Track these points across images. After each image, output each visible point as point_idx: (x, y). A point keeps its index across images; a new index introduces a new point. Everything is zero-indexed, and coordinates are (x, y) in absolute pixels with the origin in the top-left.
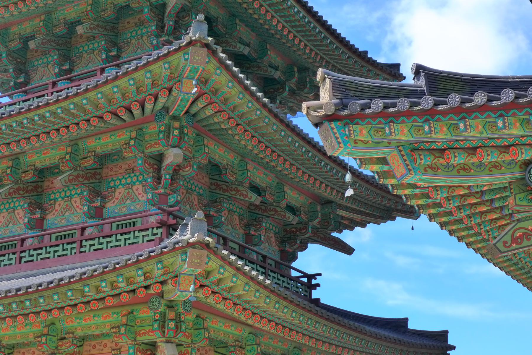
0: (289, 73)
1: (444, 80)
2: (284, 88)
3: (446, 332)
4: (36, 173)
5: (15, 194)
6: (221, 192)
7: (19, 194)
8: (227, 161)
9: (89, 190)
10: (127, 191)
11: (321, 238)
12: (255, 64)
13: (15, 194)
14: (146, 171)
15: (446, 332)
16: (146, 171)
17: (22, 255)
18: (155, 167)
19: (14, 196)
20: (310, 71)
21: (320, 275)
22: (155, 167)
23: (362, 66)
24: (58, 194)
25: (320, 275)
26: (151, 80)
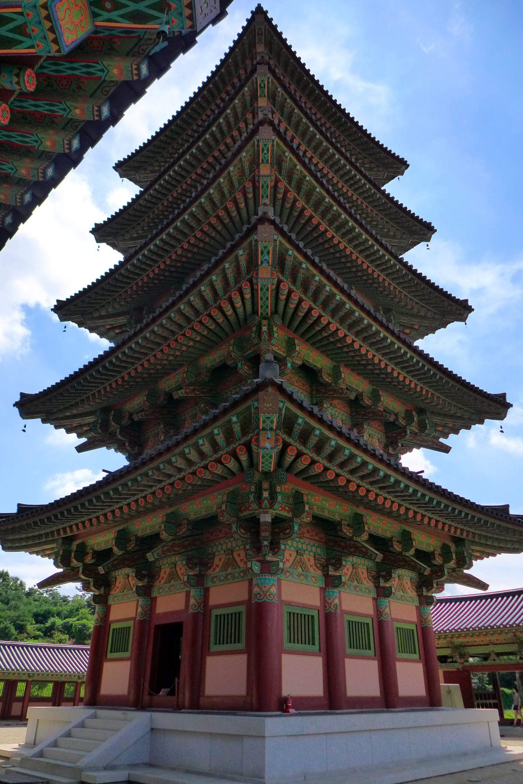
0: (409, 416)
1: (229, 634)
2: (406, 432)
3: (508, 506)
4: (138, 543)
5: (170, 552)
6: (339, 549)
7: (175, 551)
8: (340, 516)
9: (187, 560)
10: (227, 557)
11: (454, 577)
12: (331, 388)
13: (170, 552)
14: (242, 537)
15: (508, 506)
16: (242, 537)
18: (253, 530)
19: (168, 554)
20: (428, 412)
22: (253, 530)
23: (483, 402)
24: (220, 546)
26: (317, 438)
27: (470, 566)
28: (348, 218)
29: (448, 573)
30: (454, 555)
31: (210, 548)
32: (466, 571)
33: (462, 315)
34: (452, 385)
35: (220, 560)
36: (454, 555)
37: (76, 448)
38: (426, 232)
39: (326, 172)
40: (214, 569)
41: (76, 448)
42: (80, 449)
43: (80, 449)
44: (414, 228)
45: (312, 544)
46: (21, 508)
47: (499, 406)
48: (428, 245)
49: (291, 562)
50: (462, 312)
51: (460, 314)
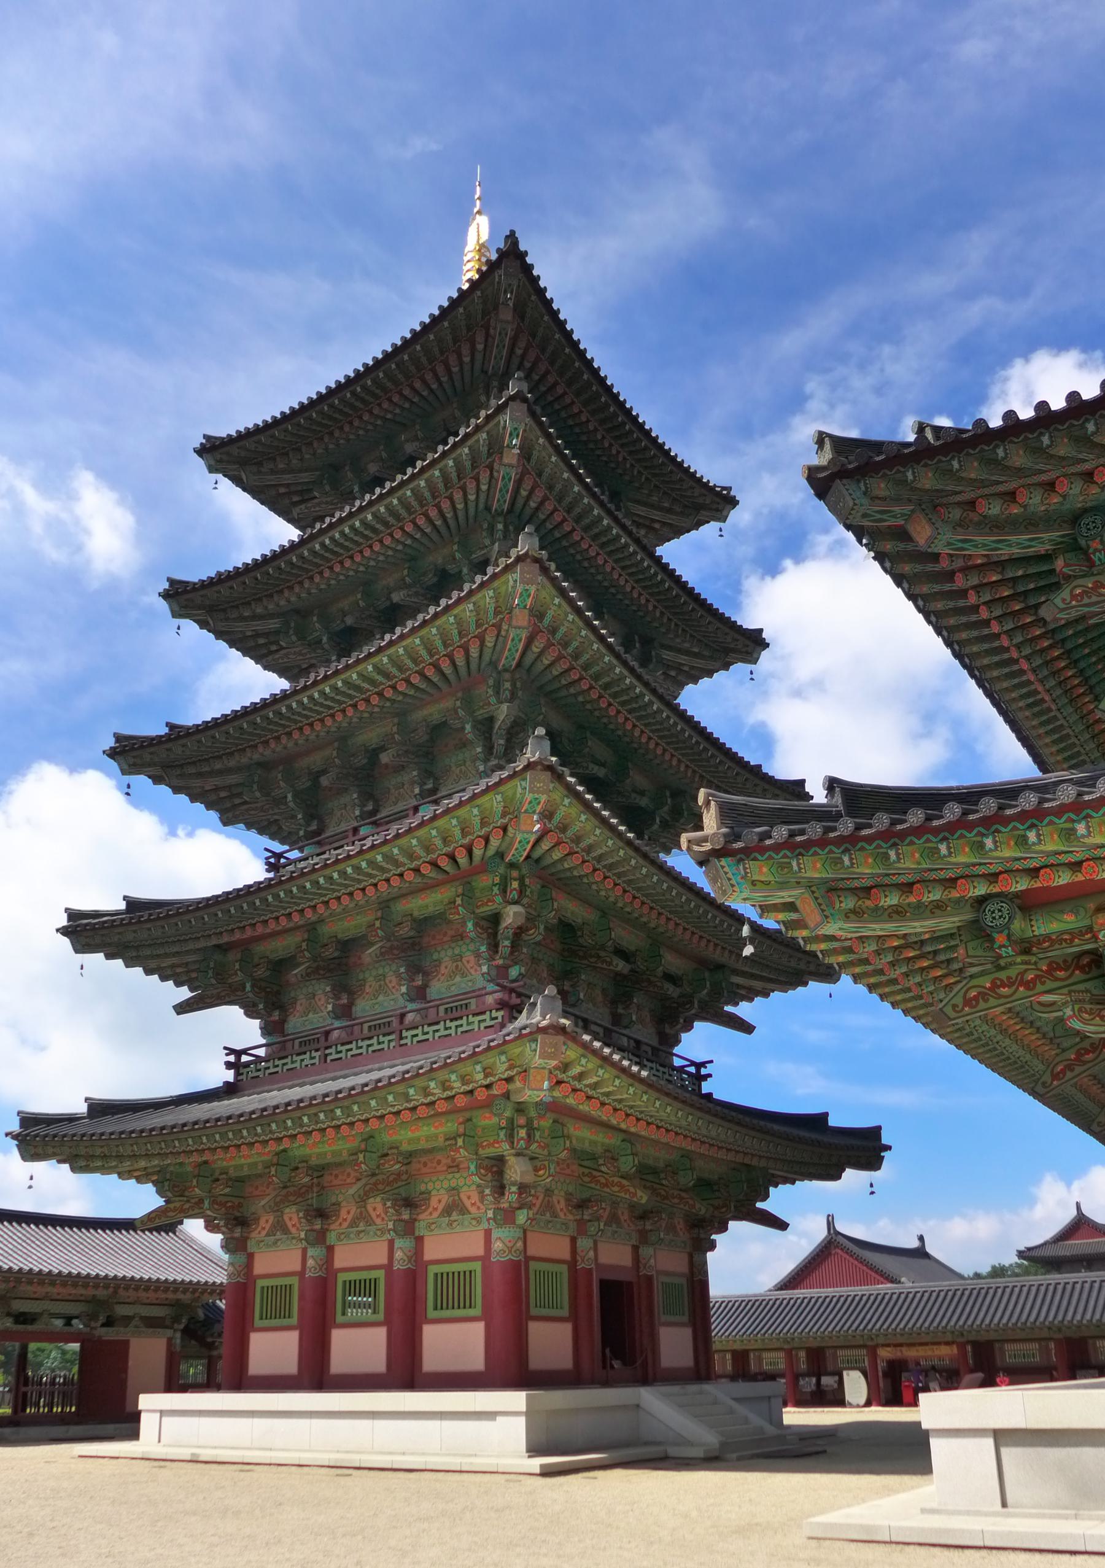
17: (327, 1052)
21: (711, 1062)
25: (711, 1062)
27: (765, 1197)
28: (592, 502)
29: (735, 1207)
30: (708, 983)
31: (423, 1185)
32: (759, 1205)
33: (721, 511)
34: (729, 768)
35: (440, 1201)
36: (708, 983)
37: (174, 1007)
38: (720, 507)
39: (569, 529)
40: (431, 1214)
41: (174, 1007)
42: (182, 1008)
43: (182, 1008)
44: (701, 500)
45: (562, 1180)
46: (133, 905)
47: (748, 642)
48: (721, 530)
49: (538, 1205)
50: (720, 507)
51: (717, 510)
